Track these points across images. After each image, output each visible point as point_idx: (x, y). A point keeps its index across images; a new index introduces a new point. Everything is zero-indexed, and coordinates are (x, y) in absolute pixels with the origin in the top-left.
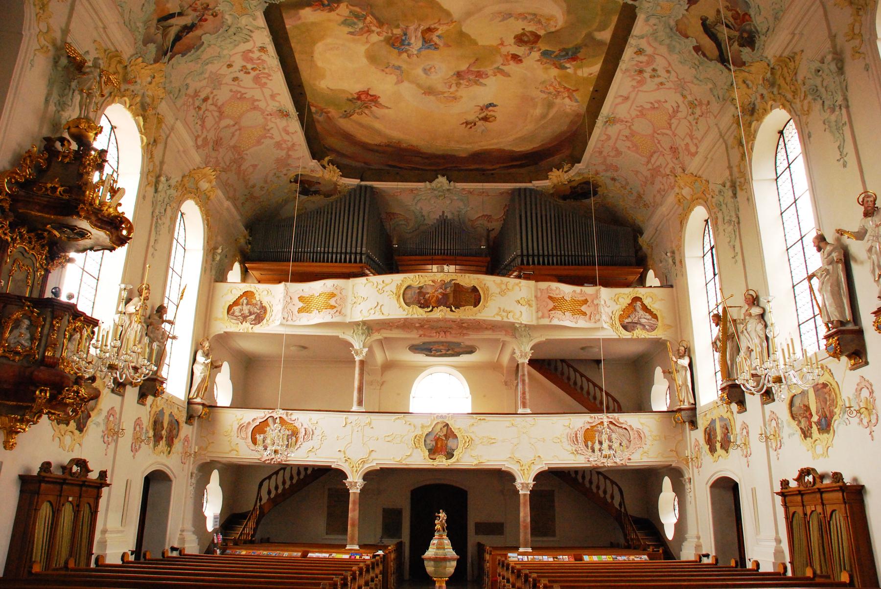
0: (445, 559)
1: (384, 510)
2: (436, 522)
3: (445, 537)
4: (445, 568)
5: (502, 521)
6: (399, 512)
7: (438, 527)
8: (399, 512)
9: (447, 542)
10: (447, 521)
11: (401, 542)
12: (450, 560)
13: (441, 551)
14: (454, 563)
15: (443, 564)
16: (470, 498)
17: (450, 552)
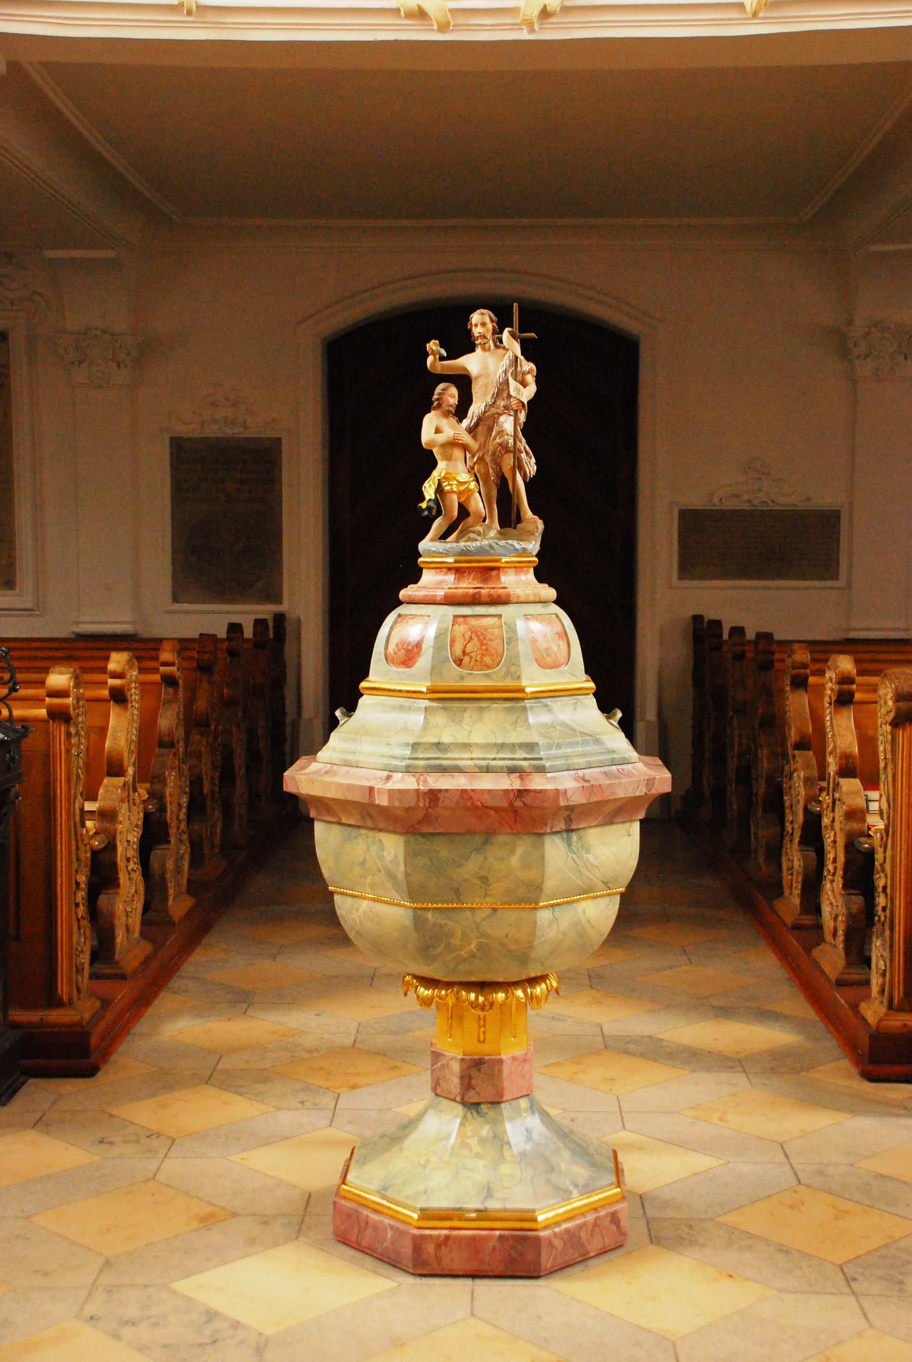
0: (525, 815)
1: (178, 446)
2: (434, 429)
3: (522, 582)
4: (530, 896)
5: (824, 498)
6: (257, 463)
7: (452, 477)
8: (257, 463)
9: (539, 630)
10: (539, 423)
11: (280, 618)
12: (571, 817)
13: (482, 730)
14: (617, 849)
15: (510, 857)
16: (645, 354)
17: (582, 744)
